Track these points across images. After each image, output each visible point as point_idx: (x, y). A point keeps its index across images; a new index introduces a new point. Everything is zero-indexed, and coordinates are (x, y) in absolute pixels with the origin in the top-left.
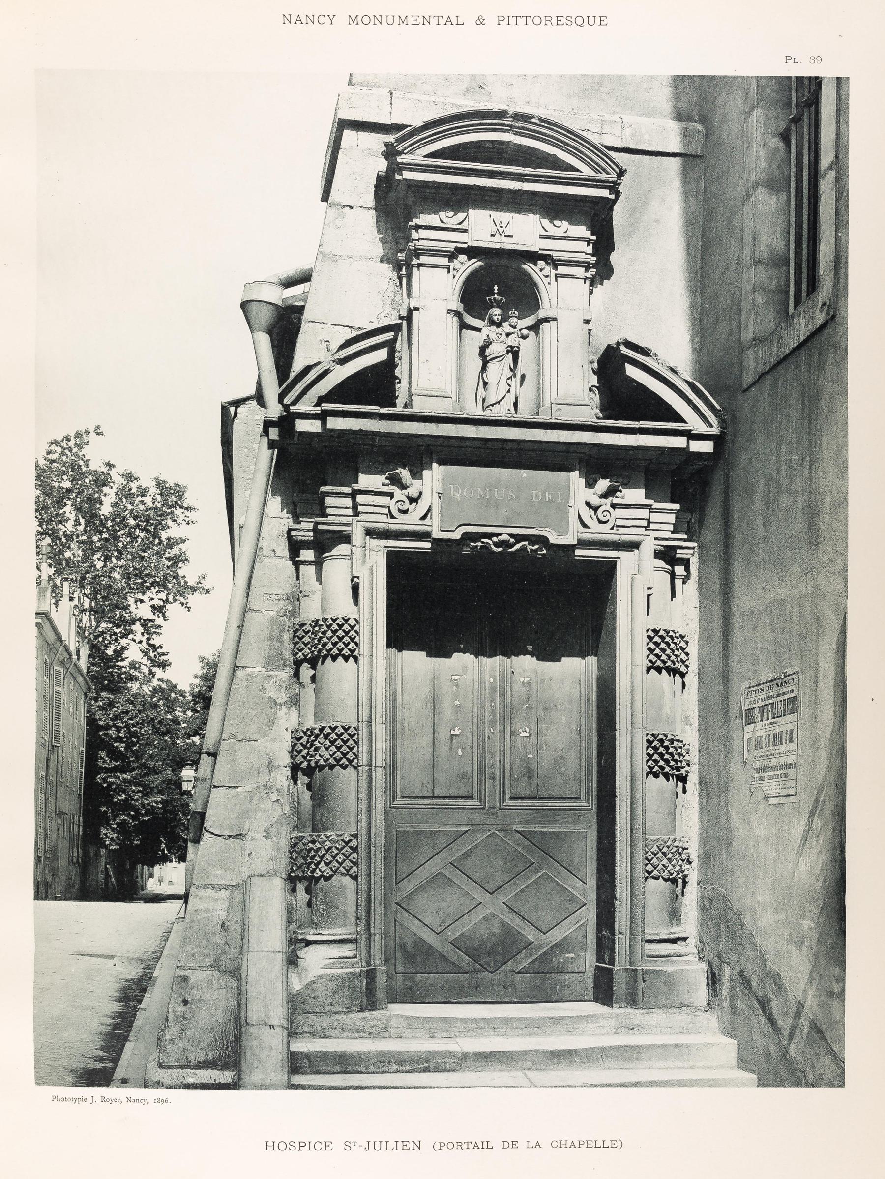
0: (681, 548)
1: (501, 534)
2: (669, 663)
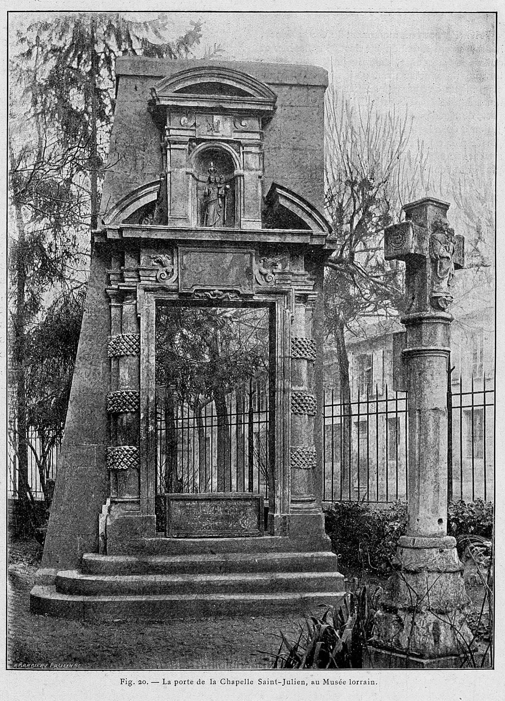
0: (310, 294)
1: (215, 290)
2: (304, 356)
